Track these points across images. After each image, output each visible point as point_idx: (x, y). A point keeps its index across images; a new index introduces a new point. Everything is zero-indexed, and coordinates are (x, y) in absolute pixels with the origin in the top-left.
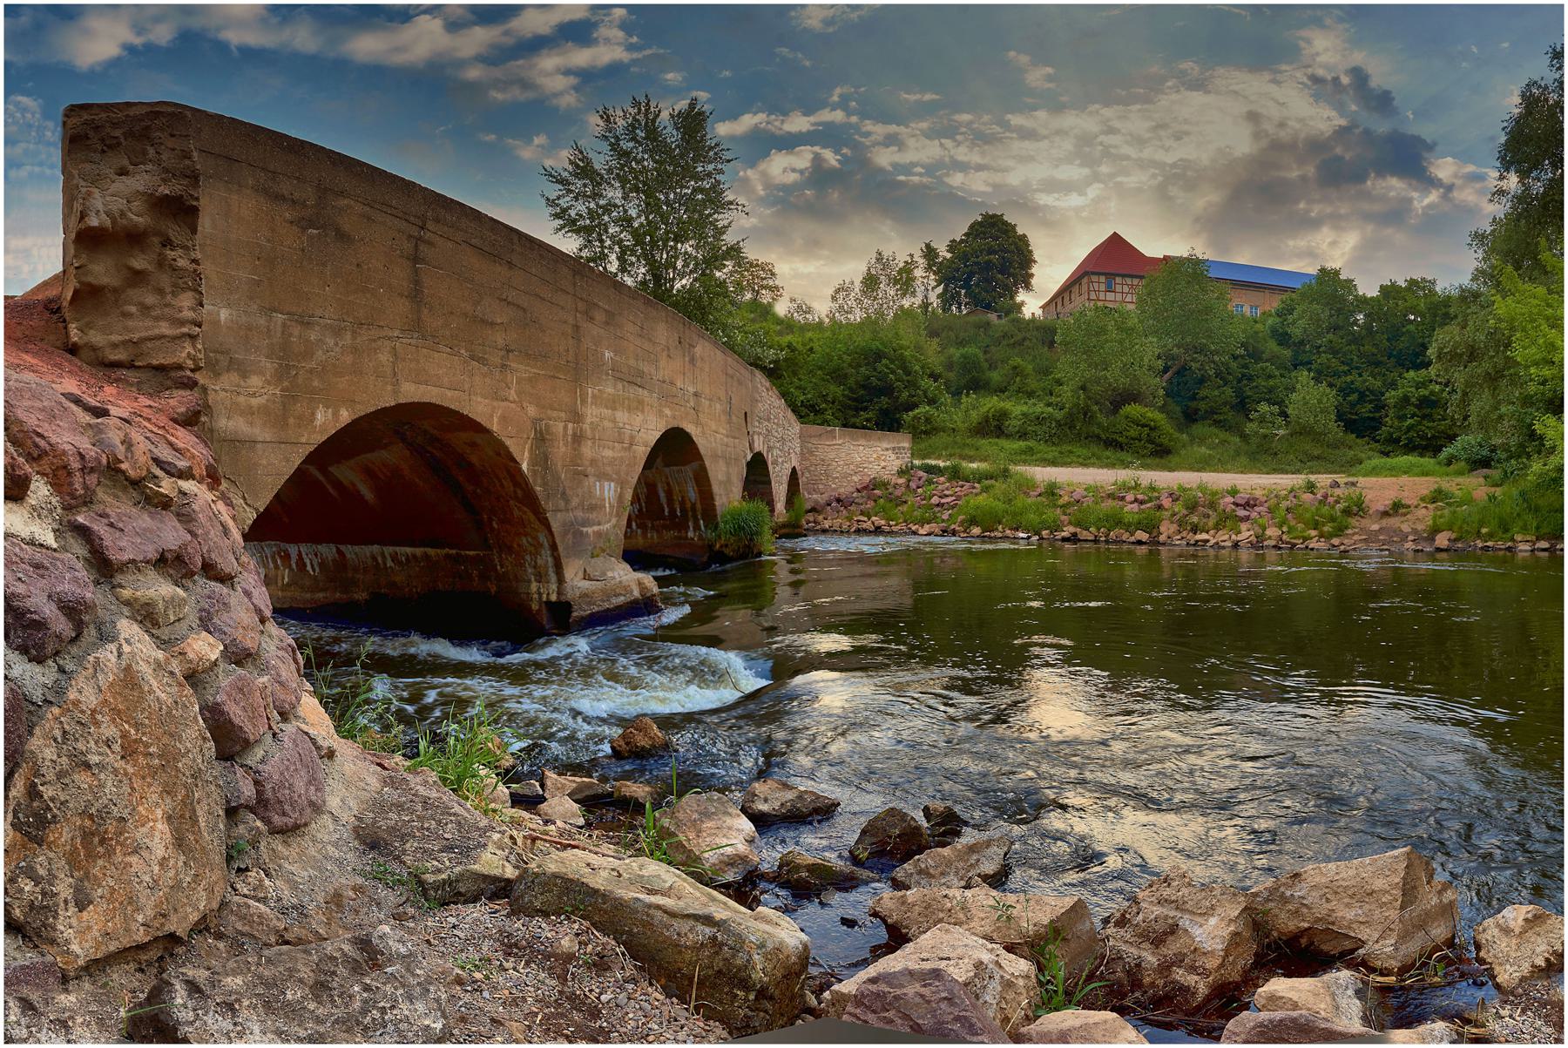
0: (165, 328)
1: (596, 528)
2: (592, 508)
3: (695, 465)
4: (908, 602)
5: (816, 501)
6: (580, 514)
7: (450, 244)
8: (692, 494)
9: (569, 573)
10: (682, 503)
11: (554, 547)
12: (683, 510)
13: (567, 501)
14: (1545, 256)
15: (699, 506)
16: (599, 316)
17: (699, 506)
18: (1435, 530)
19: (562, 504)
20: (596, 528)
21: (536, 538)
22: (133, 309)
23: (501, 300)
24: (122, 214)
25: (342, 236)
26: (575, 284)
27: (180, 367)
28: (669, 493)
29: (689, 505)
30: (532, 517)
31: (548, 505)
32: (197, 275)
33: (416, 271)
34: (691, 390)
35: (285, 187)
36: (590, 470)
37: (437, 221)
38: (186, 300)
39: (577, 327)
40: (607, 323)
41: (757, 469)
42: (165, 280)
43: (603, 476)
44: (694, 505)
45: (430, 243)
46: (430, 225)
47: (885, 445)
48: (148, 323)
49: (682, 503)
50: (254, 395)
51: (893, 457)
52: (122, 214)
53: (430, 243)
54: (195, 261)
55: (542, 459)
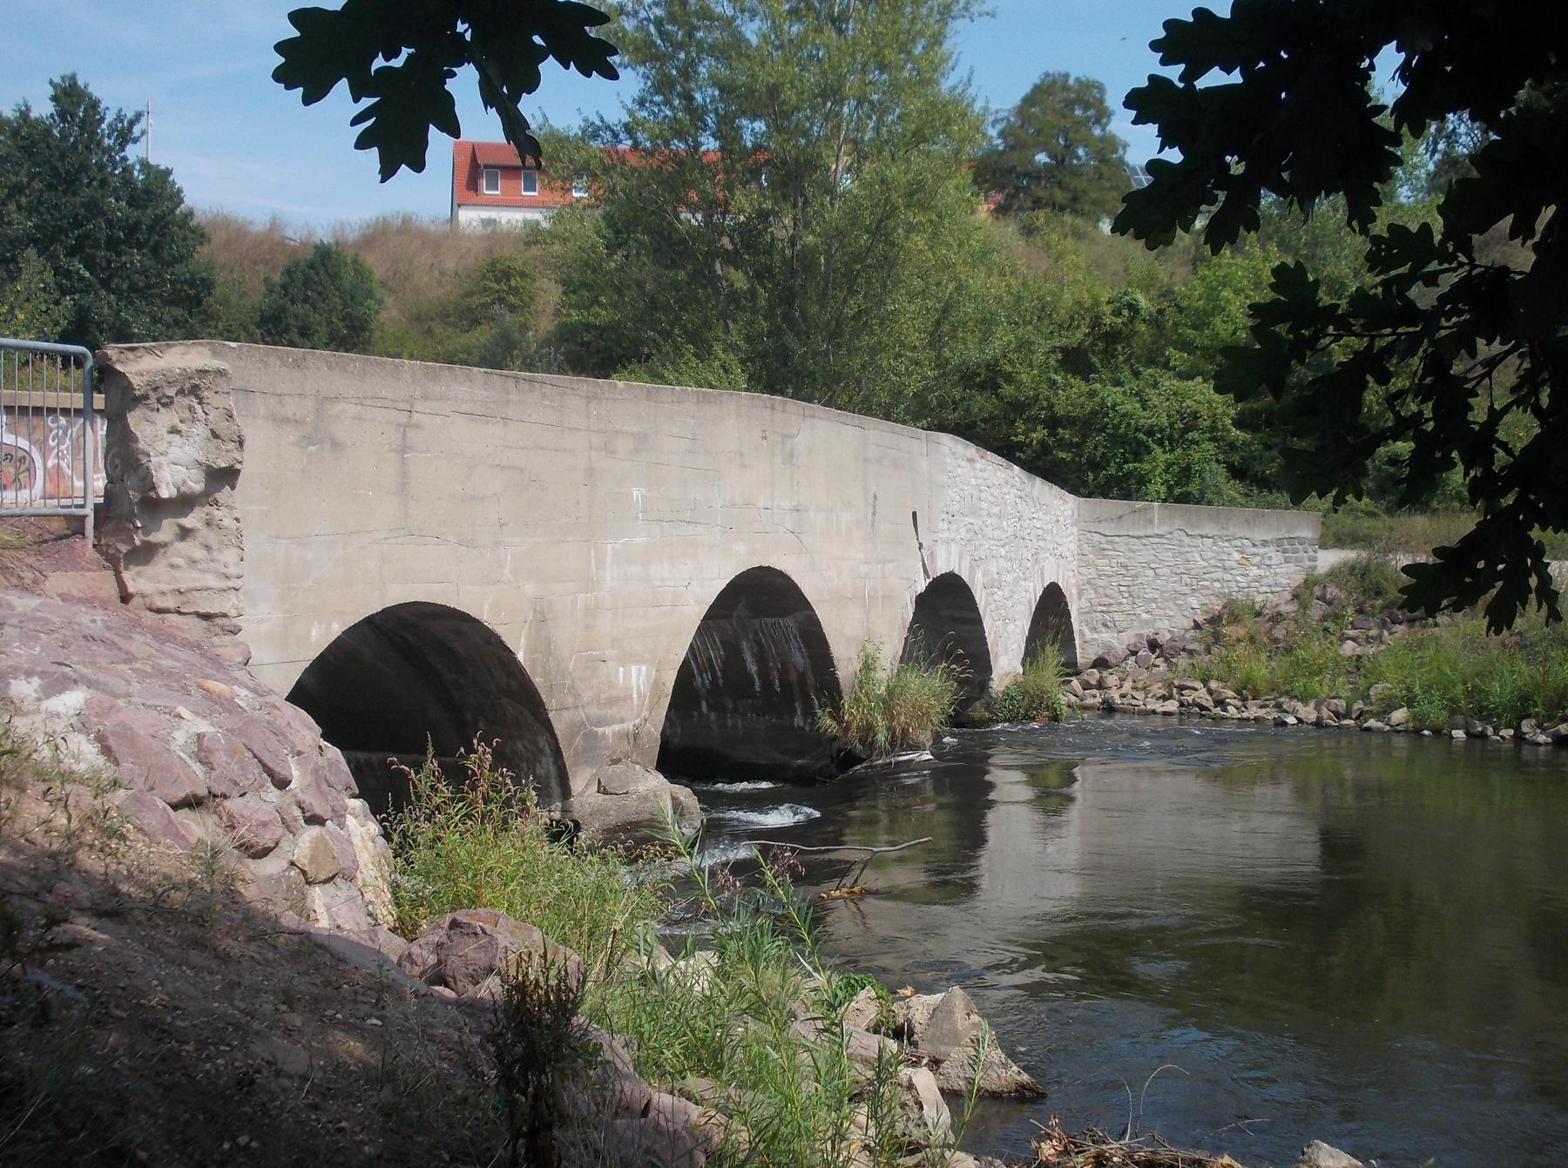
0: (212, 581)
1: (617, 727)
2: (612, 702)
3: (800, 616)
4: (1306, 853)
5: (1109, 648)
6: (594, 711)
7: (438, 420)
8: (799, 658)
9: (577, 784)
10: (784, 673)
11: (557, 753)
12: (785, 683)
13: (577, 696)
14: (716, 655)
15: (810, 679)
16: (624, 445)
17: (810, 679)
18: (1520, 708)
19: (570, 700)
20: (617, 727)
21: (535, 743)
22: (181, 561)
23: (493, 466)
24: (184, 482)
25: (337, 445)
26: (588, 416)
27: (225, 615)
28: (761, 659)
29: (793, 677)
30: (530, 718)
31: (551, 704)
32: (239, 535)
33: (404, 462)
34: (787, 504)
35: (290, 408)
36: (610, 653)
37: (425, 397)
38: (230, 556)
39: (591, 471)
40: (636, 451)
41: (946, 611)
42: (211, 537)
43: (626, 659)
44: (802, 676)
45: (418, 426)
46: (419, 406)
47: (1259, 535)
48: (195, 574)
49: (784, 673)
50: (261, 621)
51: (1277, 558)
52: (184, 482)
53: (418, 426)
54: (237, 520)
55: (543, 645)
